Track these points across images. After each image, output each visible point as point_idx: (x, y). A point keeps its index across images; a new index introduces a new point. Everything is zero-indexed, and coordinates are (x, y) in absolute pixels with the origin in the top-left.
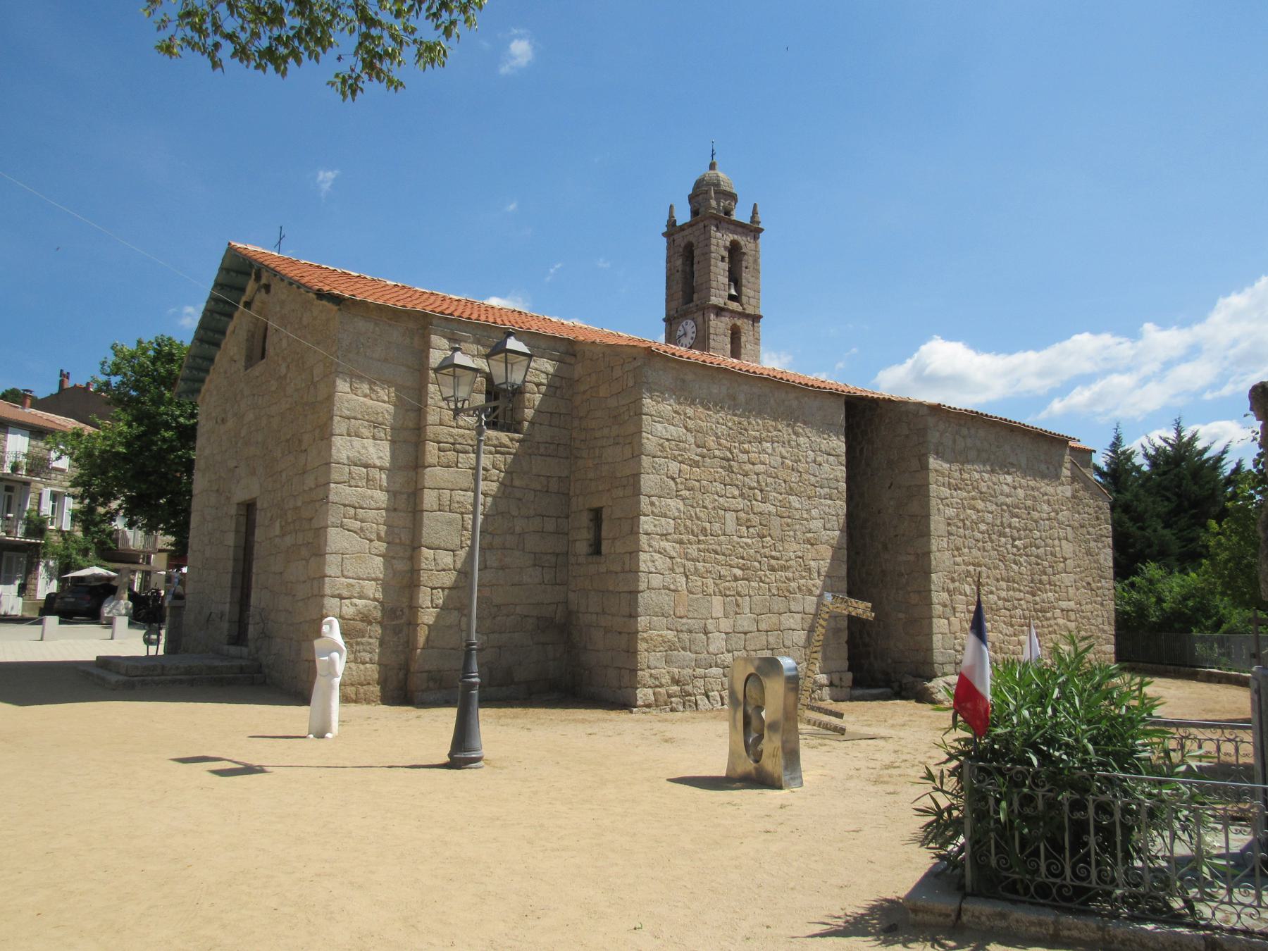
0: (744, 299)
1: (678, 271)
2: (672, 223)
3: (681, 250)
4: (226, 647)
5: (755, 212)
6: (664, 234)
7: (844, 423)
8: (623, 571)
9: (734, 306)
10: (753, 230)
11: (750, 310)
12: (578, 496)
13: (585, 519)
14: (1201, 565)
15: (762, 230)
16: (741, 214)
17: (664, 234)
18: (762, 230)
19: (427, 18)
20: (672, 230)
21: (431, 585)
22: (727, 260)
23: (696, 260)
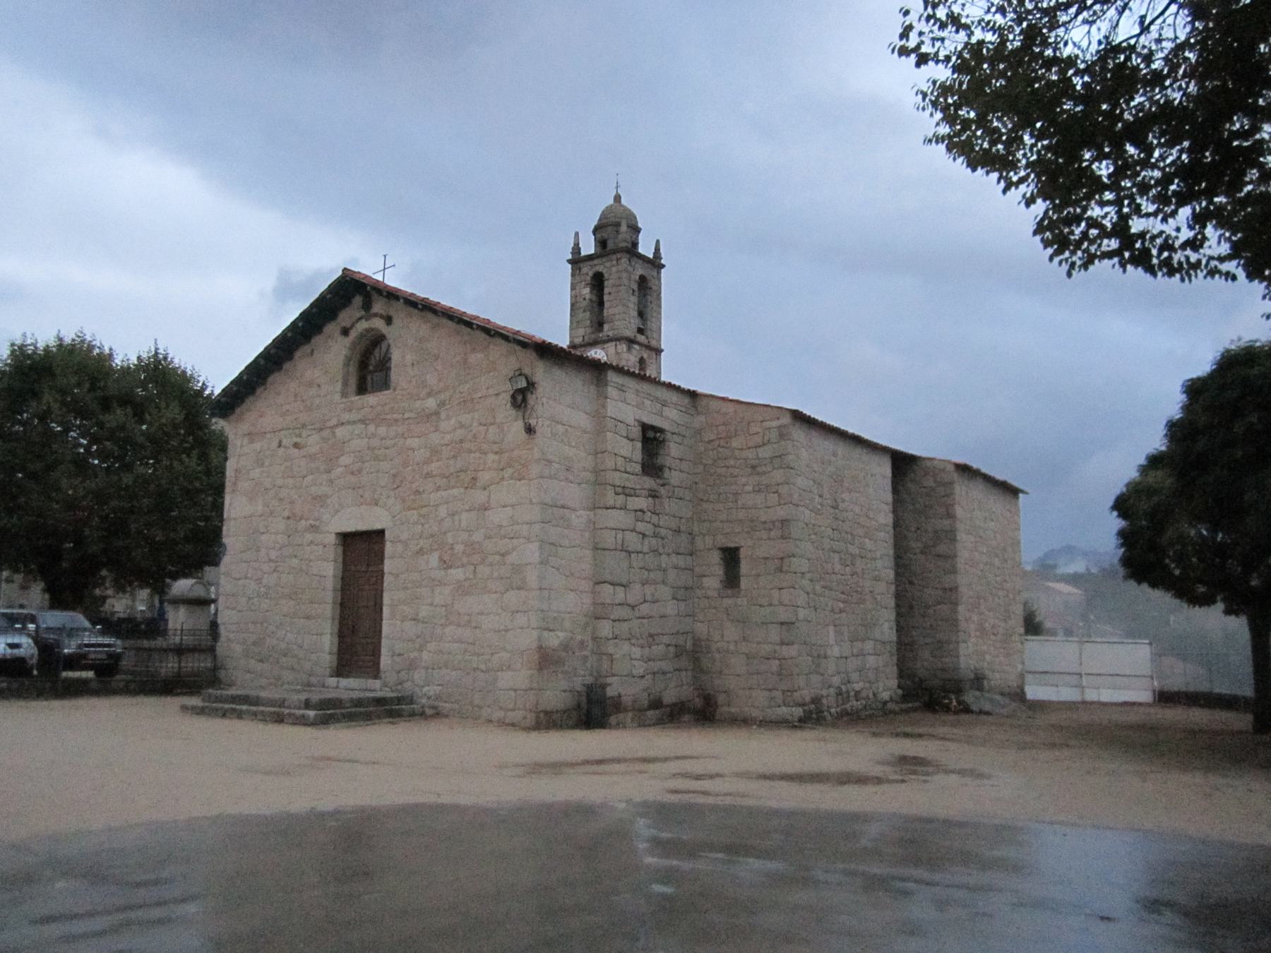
0: (649, 333)
1: (585, 299)
2: (576, 249)
3: (589, 278)
4: (332, 681)
5: (657, 250)
6: (569, 261)
7: (890, 475)
8: (771, 605)
9: (641, 338)
10: (655, 263)
11: (653, 343)
12: (704, 535)
13: (716, 557)
14: (104, 578)
15: (663, 266)
16: (646, 249)
17: (569, 261)
18: (663, 266)
19: (1205, 277)
20: (577, 261)
21: (612, 617)
22: (637, 293)
23: (606, 291)
